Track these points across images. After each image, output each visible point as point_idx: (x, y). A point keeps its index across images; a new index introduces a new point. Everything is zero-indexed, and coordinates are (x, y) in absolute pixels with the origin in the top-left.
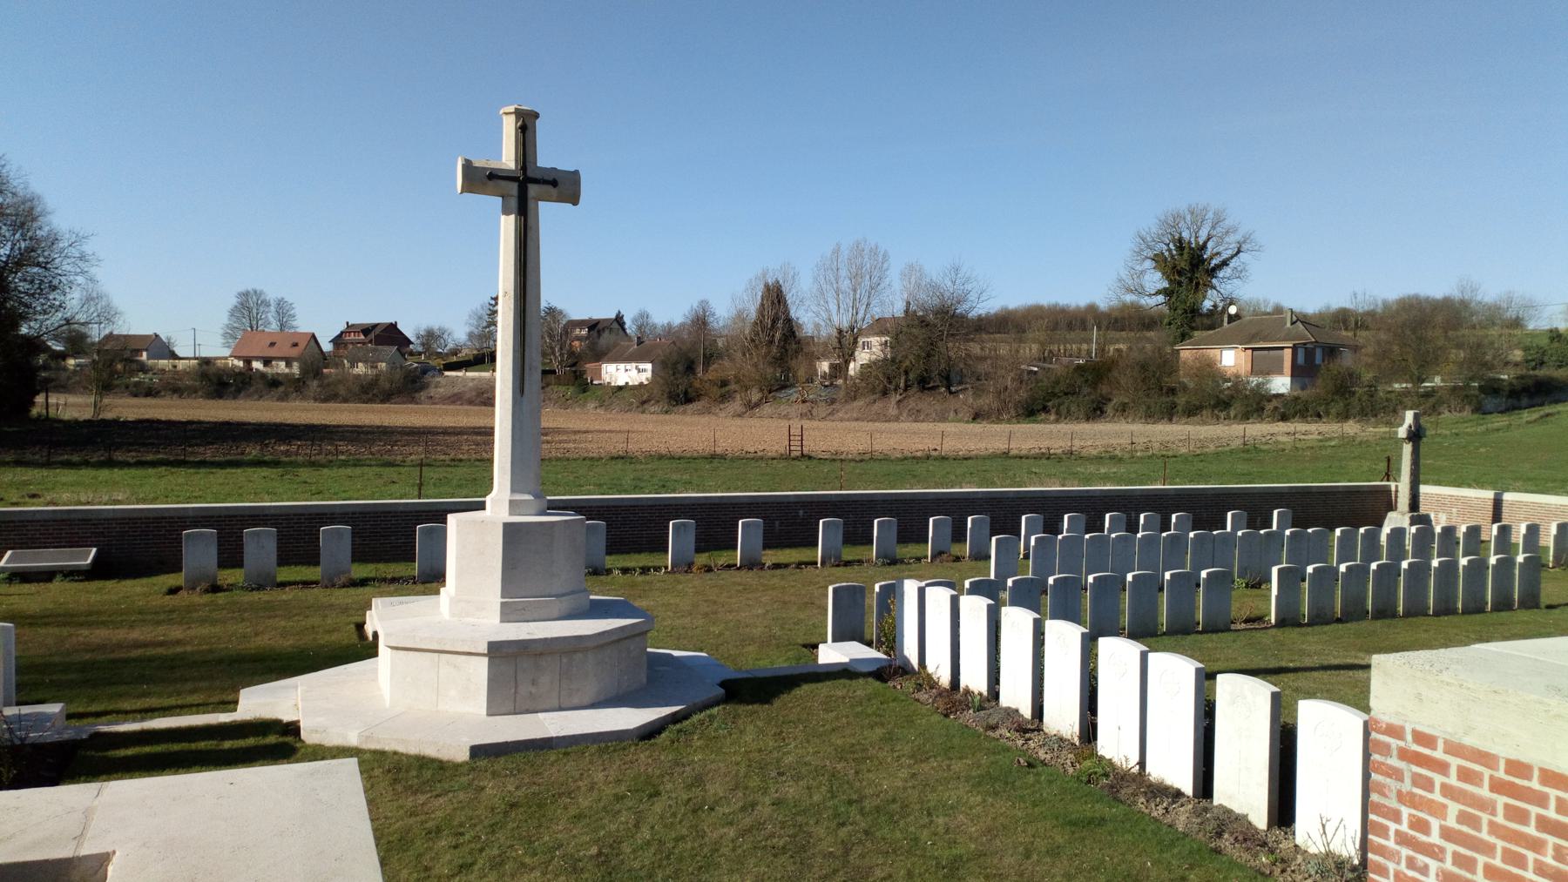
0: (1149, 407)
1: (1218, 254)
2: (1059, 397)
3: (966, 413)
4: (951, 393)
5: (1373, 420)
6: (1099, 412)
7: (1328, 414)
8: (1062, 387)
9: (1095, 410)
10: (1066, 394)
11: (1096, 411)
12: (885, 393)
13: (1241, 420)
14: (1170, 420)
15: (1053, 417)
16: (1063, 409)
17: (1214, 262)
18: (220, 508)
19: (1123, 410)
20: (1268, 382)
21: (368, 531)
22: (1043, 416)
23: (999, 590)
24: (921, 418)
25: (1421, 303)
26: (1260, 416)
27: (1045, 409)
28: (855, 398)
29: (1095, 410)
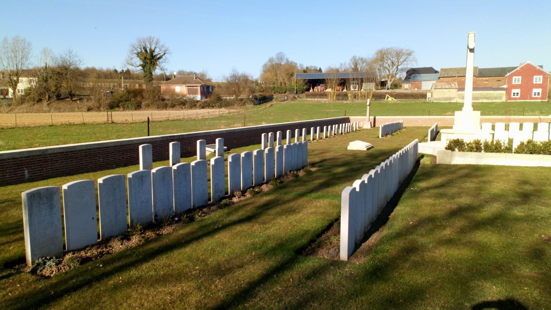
0: (158, 105)
1: (160, 54)
2: (123, 102)
3: (85, 108)
4: (73, 101)
5: (229, 108)
6: (139, 107)
7: (215, 106)
8: (124, 98)
9: (138, 106)
10: (126, 101)
11: (138, 107)
12: (40, 100)
13: (190, 109)
14: (166, 109)
15: (122, 109)
16: (126, 106)
17: (158, 56)
18: (264, 168)
19: (148, 106)
20: (197, 96)
21: (50, 172)
22: (117, 109)
23: (214, 165)
24: (62, 111)
25: (158, 77)
26: (196, 107)
27: (118, 106)
28: (22, 103)
29: (138, 106)
